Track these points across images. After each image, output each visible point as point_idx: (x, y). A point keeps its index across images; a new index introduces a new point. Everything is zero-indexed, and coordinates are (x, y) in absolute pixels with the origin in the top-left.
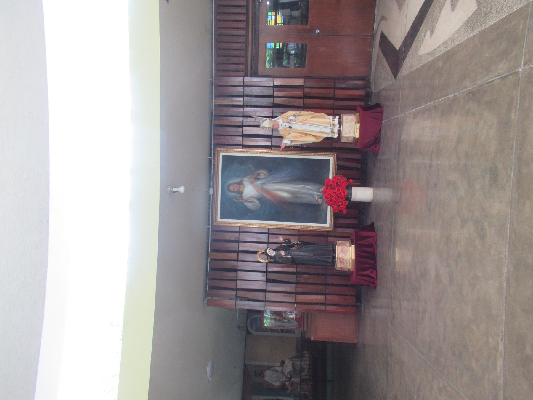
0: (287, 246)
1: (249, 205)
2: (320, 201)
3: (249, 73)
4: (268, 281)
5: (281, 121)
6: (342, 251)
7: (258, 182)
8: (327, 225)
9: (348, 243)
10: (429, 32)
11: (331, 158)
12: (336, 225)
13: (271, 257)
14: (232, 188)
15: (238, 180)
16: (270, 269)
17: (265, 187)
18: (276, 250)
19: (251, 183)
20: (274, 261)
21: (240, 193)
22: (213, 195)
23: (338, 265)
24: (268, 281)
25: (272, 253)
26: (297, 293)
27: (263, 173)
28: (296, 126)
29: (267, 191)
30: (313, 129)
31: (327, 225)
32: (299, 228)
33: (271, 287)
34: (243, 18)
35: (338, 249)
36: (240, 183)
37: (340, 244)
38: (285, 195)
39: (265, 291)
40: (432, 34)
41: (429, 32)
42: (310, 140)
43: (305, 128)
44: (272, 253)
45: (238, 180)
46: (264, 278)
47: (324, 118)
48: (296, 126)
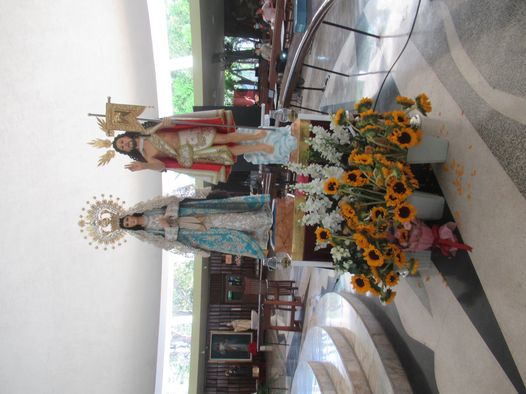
0: (236, 369)
1: (222, 353)
2: (248, 350)
3: (223, 275)
4: (229, 383)
5: (234, 323)
6: (255, 370)
7: (225, 344)
8: (250, 360)
9: (257, 367)
10: (107, 162)
11: (251, 334)
12: (253, 359)
13: (230, 374)
14: (215, 346)
15: (217, 343)
16: (229, 378)
17: (228, 346)
18: (232, 371)
19: (223, 344)
20: (231, 375)
21: (218, 348)
22: (208, 349)
23: (253, 375)
24: (229, 383)
25: (231, 372)
26: (240, 388)
27: (227, 340)
28: (239, 325)
29: (229, 347)
30: (244, 326)
31: (250, 360)
32: (240, 361)
33: (230, 386)
34: (220, 298)
35: (253, 369)
36: (219, 345)
37: (254, 368)
38: (235, 348)
39: (227, 388)
40: (108, 162)
41: (107, 162)
42: (244, 330)
43: (242, 326)
44: (231, 372)
45: (217, 343)
46: (227, 382)
47: (248, 322)
48: (239, 325)
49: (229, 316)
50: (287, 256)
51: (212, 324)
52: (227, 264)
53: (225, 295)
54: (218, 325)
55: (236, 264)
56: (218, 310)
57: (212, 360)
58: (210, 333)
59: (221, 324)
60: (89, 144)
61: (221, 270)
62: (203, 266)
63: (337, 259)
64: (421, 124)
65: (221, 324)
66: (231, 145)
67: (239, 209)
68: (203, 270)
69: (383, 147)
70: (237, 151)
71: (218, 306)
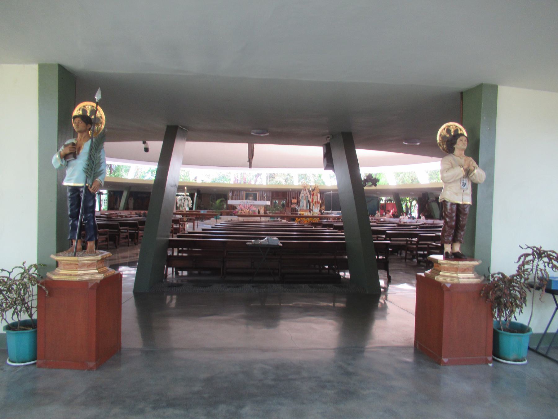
21: (250, 196)
36: (252, 196)
49: (111, 216)
50: (477, 260)
51: (262, 193)
52: (292, 200)
53: (276, 199)
54: (262, 196)
55: (292, 204)
56: (269, 196)
57: (245, 193)
58: (257, 192)
59: (262, 197)
60: (1, 323)
61: (289, 197)
62: (291, 189)
63: (101, 156)
64: (77, 143)
65: (262, 197)
66: (316, 203)
67: (307, 204)
68: (290, 189)
69: (506, 312)
70: (315, 204)
71: (271, 196)
